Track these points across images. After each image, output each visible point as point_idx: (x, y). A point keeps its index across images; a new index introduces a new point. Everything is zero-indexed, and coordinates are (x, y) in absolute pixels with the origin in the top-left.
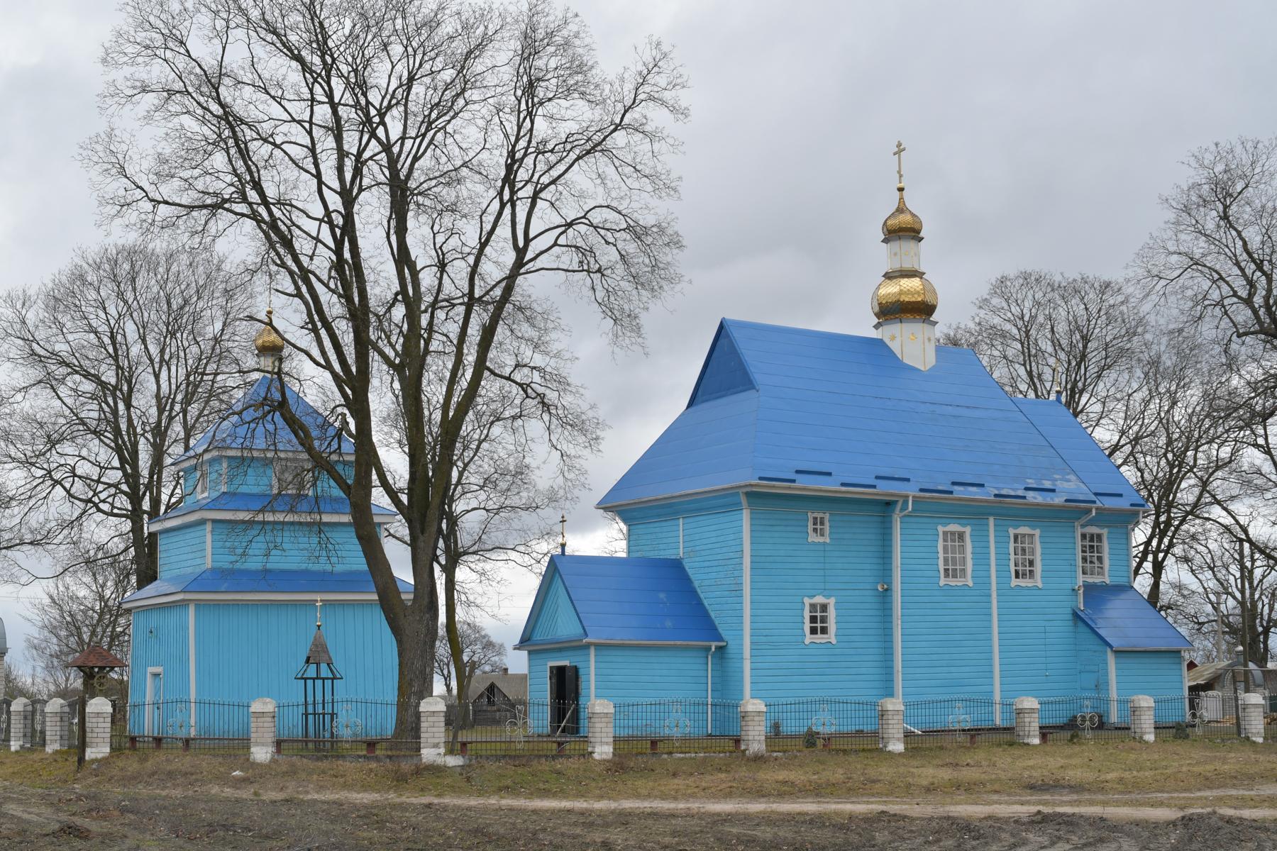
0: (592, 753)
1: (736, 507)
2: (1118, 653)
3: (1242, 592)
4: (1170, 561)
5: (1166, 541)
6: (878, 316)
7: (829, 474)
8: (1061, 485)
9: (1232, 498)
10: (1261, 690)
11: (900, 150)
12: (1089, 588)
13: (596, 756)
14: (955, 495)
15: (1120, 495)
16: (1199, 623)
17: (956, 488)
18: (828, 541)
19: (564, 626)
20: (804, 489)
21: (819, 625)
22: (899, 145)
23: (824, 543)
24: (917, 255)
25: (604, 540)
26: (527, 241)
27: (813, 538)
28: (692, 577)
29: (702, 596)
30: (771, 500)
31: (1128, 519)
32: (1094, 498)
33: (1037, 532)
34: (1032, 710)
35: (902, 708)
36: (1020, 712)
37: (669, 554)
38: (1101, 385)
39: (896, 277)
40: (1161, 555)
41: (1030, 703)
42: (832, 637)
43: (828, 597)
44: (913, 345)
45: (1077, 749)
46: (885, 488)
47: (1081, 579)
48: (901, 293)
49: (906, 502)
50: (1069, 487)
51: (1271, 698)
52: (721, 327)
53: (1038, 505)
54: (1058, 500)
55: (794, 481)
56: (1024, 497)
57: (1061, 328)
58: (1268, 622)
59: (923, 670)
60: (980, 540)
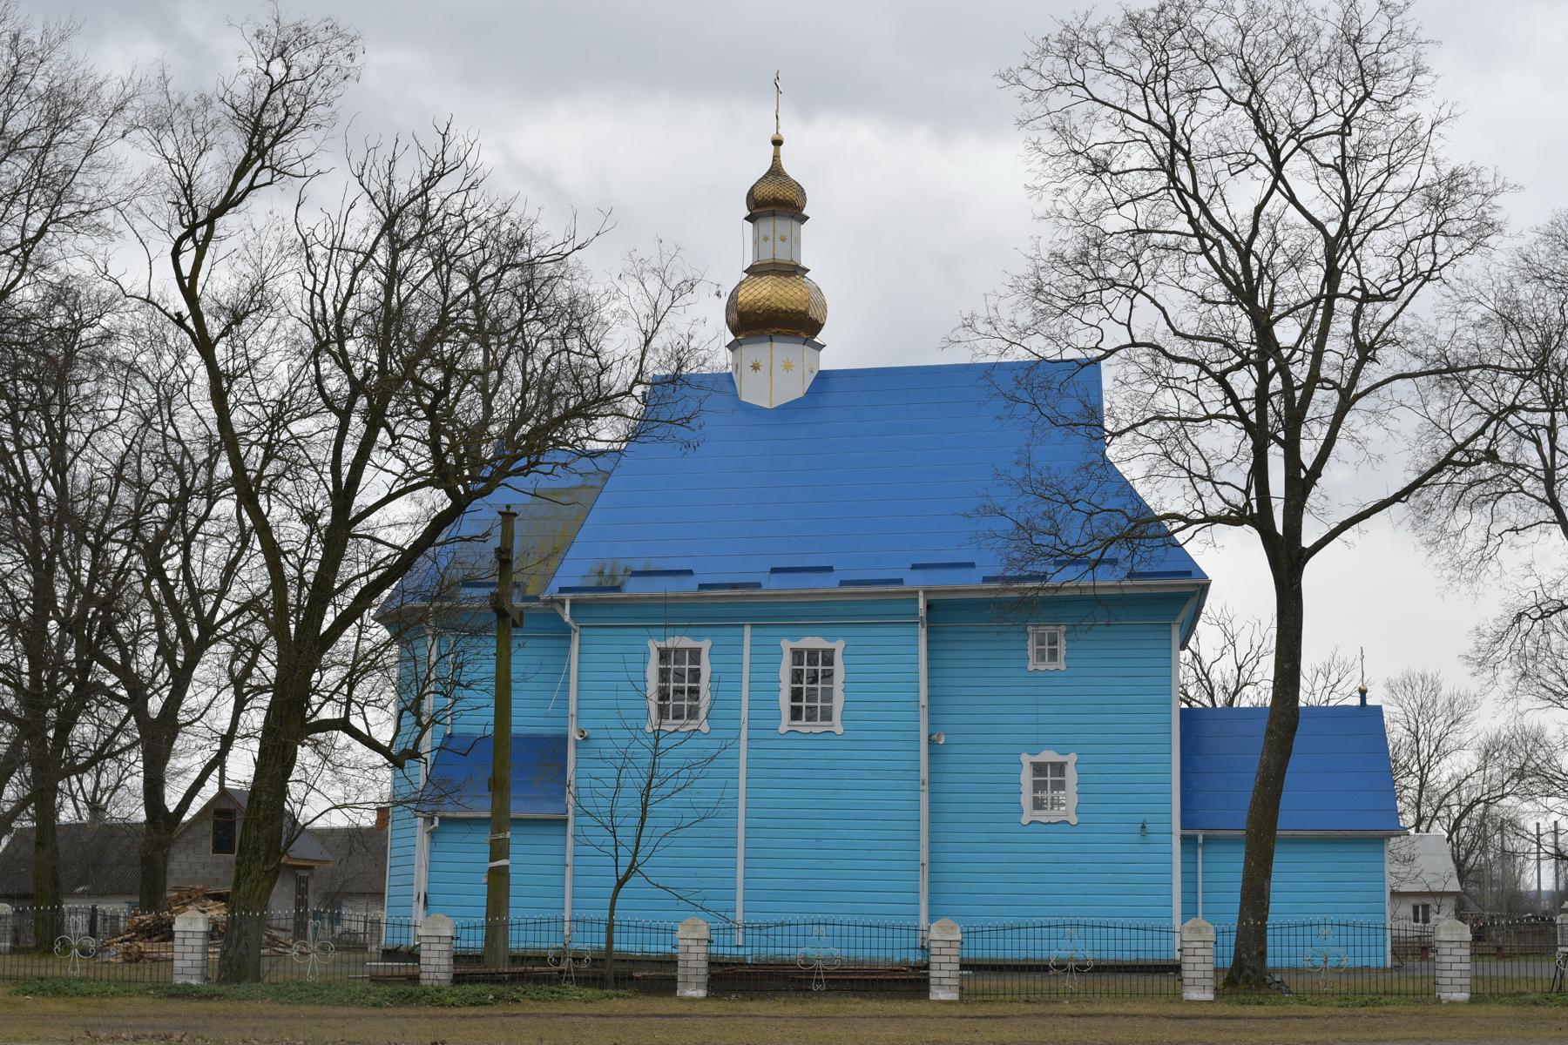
6: (734, 331)
18: (1063, 667)
26: (1278, 152)
44: (776, 376)
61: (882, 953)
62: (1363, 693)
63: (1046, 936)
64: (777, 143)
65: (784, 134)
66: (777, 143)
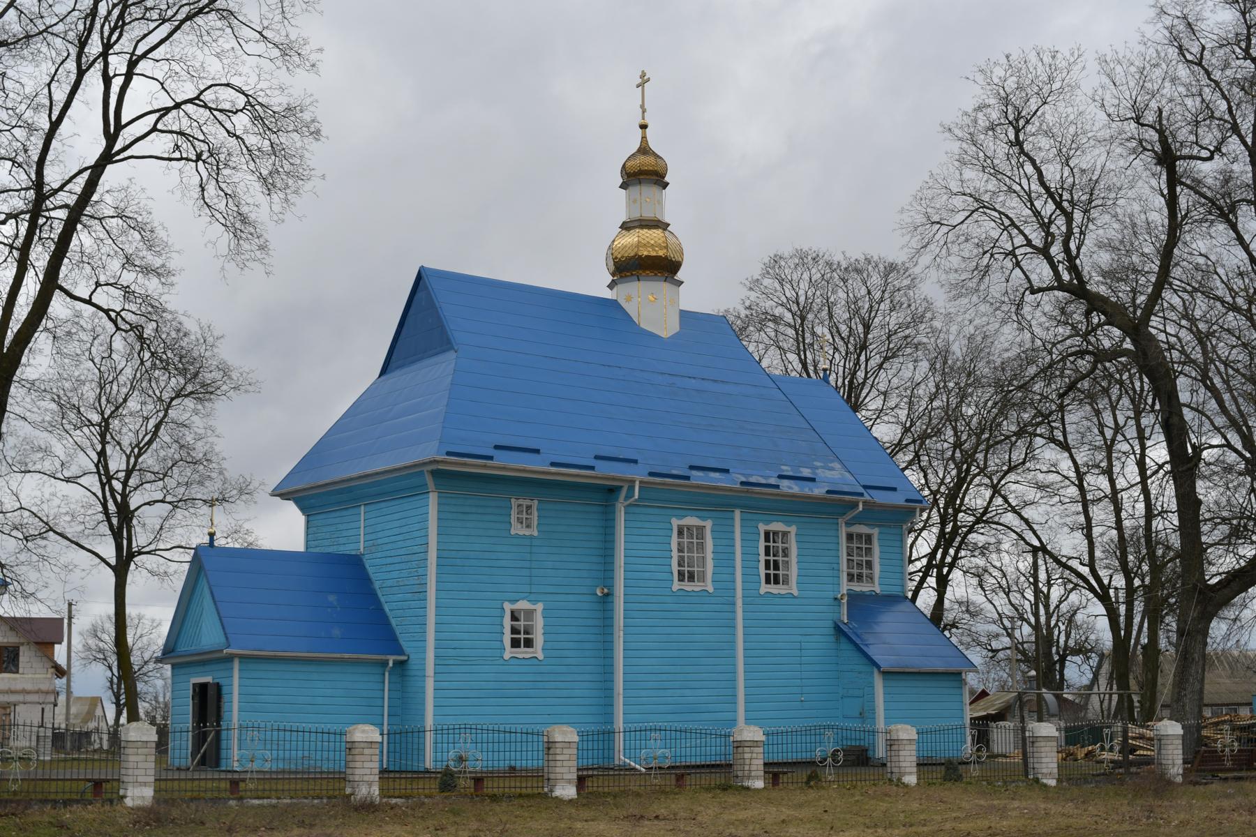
0: (124, 797)
1: (421, 491)
2: (887, 674)
3: (1036, 614)
4: (956, 575)
5: (952, 551)
6: (613, 274)
7: (537, 451)
8: (822, 474)
9: (1026, 504)
10: (1055, 720)
11: (644, 81)
12: (854, 597)
13: (129, 802)
14: (693, 482)
15: (894, 489)
16: (992, 651)
17: (694, 473)
18: (536, 533)
19: (209, 635)
20: (504, 468)
21: (522, 636)
22: (643, 75)
23: (531, 537)
24: (660, 202)
25: (283, 529)
26: (119, 127)
27: (517, 529)
28: (373, 577)
29: (382, 599)
30: (466, 481)
31: (900, 518)
32: (861, 490)
33: (793, 529)
34: (755, 744)
35: (576, 739)
36: (739, 745)
37: (348, 549)
38: (882, 374)
39: (634, 227)
40: (945, 570)
41: (753, 733)
42: (538, 650)
43: (535, 602)
44: (650, 307)
45: (812, 794)
46: (606, 470)
47: (845, 586)
48: (639, 244)
49: (631, 488)
50: (832, 476)
51: (1067, 730)
52: (419, 278)
53: (793, 496)
54: (818, 491)
55: (491, 458)
56: (777, 487)
57: (841, 313)
58: (1065, 650)
59: (516, 677)
60: (724, 533)
61: (502, 764)
62: (212, 535)
63: (288, 738)
64: (644, 127)
65: (648, 121)
66: (644, 127)
